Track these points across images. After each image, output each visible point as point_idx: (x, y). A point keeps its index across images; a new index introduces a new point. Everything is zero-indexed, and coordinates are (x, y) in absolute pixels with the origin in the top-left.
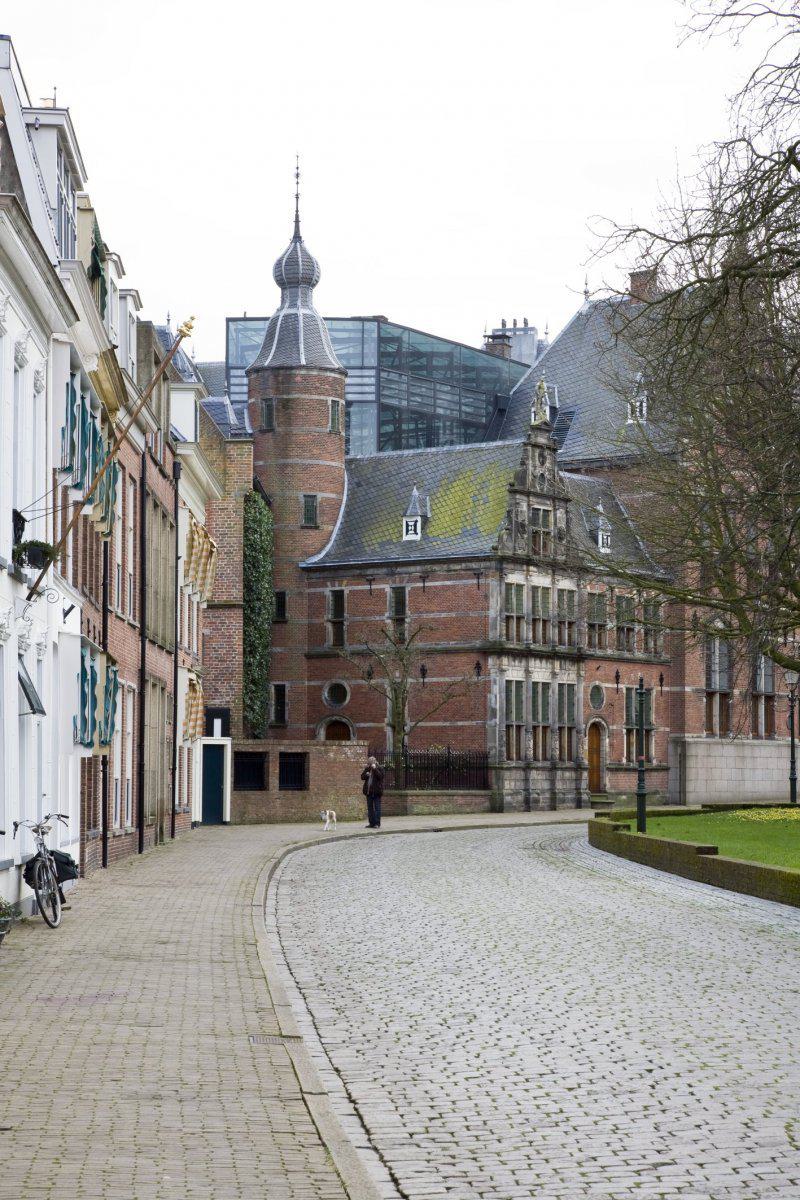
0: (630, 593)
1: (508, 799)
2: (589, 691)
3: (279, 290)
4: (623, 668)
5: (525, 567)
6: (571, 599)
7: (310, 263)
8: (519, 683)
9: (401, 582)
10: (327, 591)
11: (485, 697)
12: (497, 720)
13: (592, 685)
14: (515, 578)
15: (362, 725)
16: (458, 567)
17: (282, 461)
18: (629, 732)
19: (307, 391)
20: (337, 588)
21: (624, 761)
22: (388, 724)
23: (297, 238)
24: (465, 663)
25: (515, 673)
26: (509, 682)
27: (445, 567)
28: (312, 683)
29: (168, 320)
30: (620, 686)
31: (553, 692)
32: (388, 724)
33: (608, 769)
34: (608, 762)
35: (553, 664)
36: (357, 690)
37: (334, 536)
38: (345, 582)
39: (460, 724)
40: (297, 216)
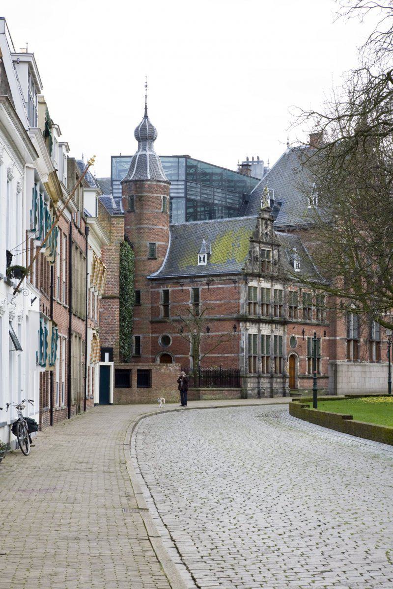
0: (310, 291)
1: (250, 392)
2: (290, 339)
3: (137, 142)
4: (306, 328)
5: (258, 278)
6: (280, 294)
7: (152, 129)
8: (255, 335)
9: (197, 286)
10: (161, 290)
11: (238, 342)
12: (244, 353)
13: (291, 336)
14: (253, 284)
15: (178, 356)
16: (225, 278)
17: (138, 226)
18: (309, 359)
19: (151, 192)
20: (166, 289)
21: (307, 373)
22: (190, 356)
23: (146, 117)
24: (228, 326)
25: (253, 330)
26: (250, 335)
27: (219, 278)
28: (154, 335)
29: (83, 157)
30: (305, 337)
31: (272, 340)
32: (190, 356)
33: (299, 377)
34: (299, 374)
35: (272, 326)
36: (175, 339)
37: (164, 263)
38: (169, 286)
39: (226, 355)
40: (146, 106)
